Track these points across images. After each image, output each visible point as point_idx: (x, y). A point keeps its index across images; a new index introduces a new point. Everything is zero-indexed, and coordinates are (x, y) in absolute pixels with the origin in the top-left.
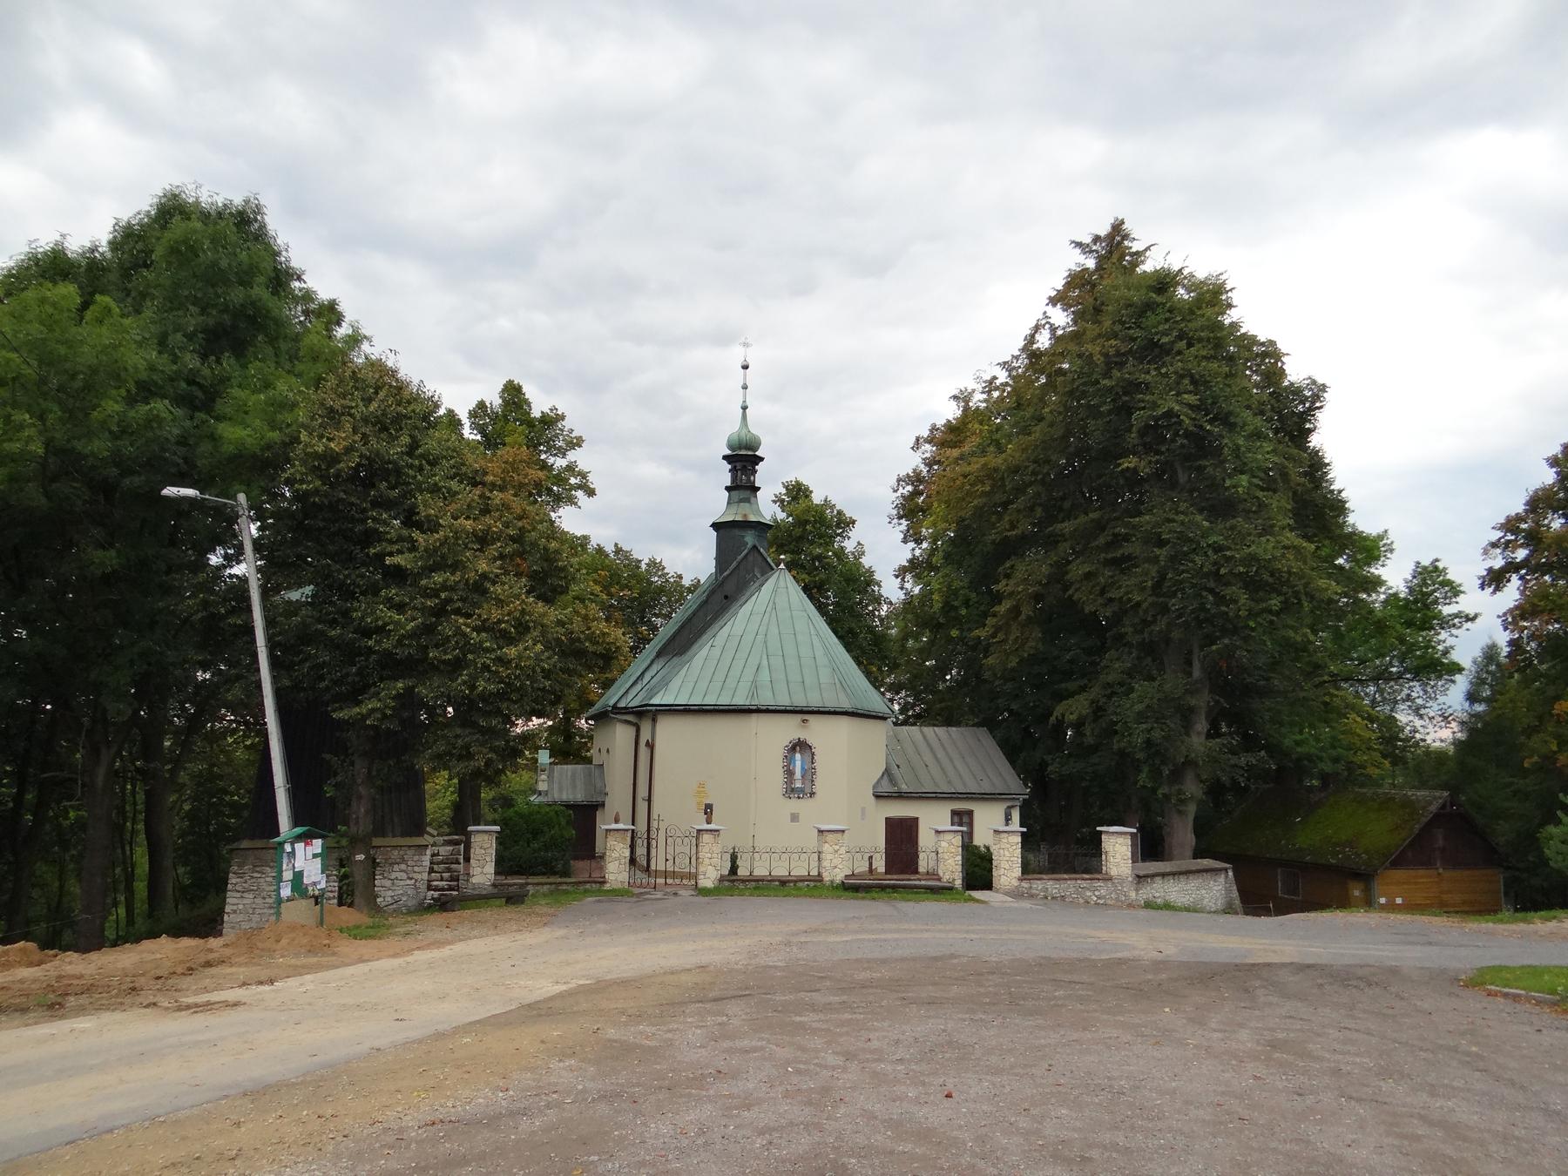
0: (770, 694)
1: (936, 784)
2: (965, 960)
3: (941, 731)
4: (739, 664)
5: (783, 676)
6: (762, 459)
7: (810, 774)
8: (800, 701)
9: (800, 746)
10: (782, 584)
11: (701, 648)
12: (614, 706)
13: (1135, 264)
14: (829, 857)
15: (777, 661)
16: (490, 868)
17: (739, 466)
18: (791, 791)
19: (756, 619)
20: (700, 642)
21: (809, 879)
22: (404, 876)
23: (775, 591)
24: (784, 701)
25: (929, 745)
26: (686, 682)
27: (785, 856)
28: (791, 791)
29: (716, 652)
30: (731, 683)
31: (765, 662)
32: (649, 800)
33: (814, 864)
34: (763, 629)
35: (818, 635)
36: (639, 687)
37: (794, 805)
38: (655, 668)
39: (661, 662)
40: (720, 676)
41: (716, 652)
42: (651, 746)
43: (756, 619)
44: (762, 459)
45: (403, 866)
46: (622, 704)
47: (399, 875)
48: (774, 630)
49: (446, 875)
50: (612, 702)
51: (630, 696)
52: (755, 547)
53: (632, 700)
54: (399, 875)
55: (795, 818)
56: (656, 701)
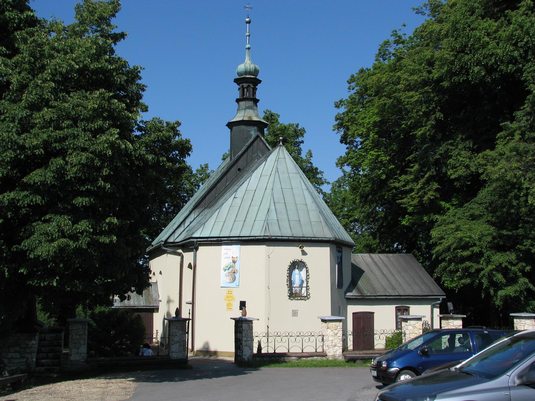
0: (277, 229)
1: (394, 288)
2: (130, 379)
3: (382, 256)
4: (255, 209)
5: (285, 217)
6: (260, 82)
7: (305, 283)
8: (298, 233)
9: (296, 265)
10: (281, 156)
11: (226, 200)
12: (166, 242)
13: (51, 314)
14: (331, 338)
15: (281, 207)
16: (84, 349)
17: (245, 85)
18: (293, 295)
19: (265, 180)
20: (226, 196)
21: (316, 354)
22: (18, 355)
23: (277, 160)
24: (287, 233)
25: (384, 263)
26: (220, 220)
27: (299, 339)
28: (293, 295)
29: (238, 201)
30: (250, 222)
31: (273, 207)
32: (193, 303)
33: (319, 344)
34: (270, 186)
35: (308, 189)
36: (181, 229)
37: (296, 304)
38: (192, 216)
39: (197, 212)
40: (242, 217)
41: (238, 201)
42: (193, 267)
43: (265, 180)
44: (260, 82)
45: (17, 348)
46: (171, 240)
47: (14, 355)
48: (278, 186)
49: (50, 355)
50: (164, 239)
51: (176, 235)
52: (258, 137)
53: (179, 237)
54: (14, 355)
55: (295, 313)
56: (196, 235)
